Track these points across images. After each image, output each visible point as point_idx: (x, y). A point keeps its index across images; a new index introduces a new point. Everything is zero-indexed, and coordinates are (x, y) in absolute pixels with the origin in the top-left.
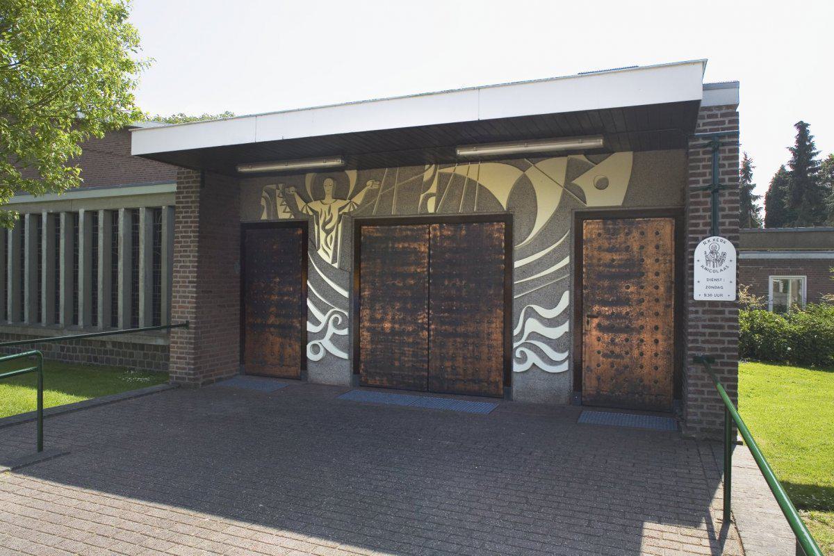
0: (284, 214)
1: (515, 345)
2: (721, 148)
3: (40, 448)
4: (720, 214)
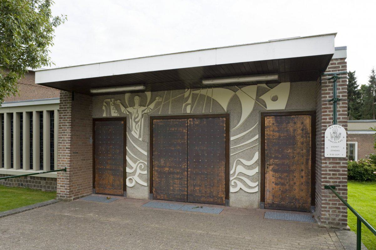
0: (114, 114)
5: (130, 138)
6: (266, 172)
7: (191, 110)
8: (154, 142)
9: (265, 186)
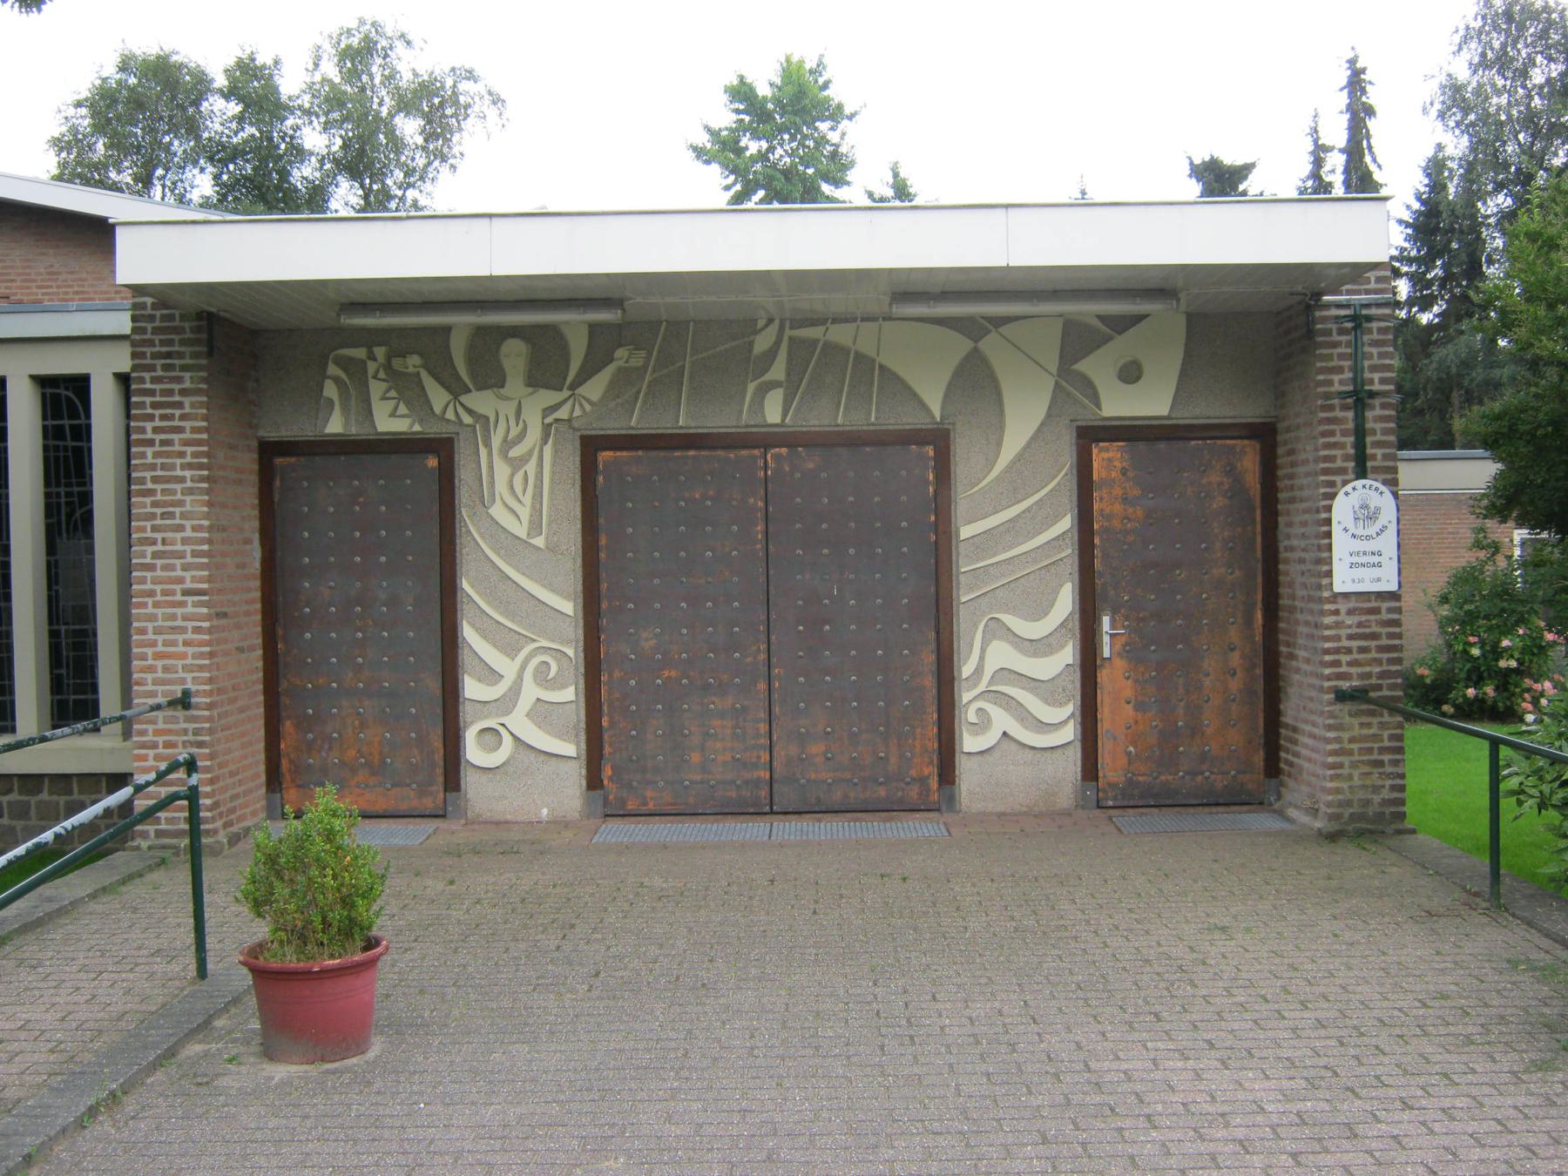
0: (390, 420)
1: (966, 697)
2: (1366, 325)
3: (202, 972)
4: (1369, 439)
6: (1098, 662)
7: (785, 413)
8: (602, 555)
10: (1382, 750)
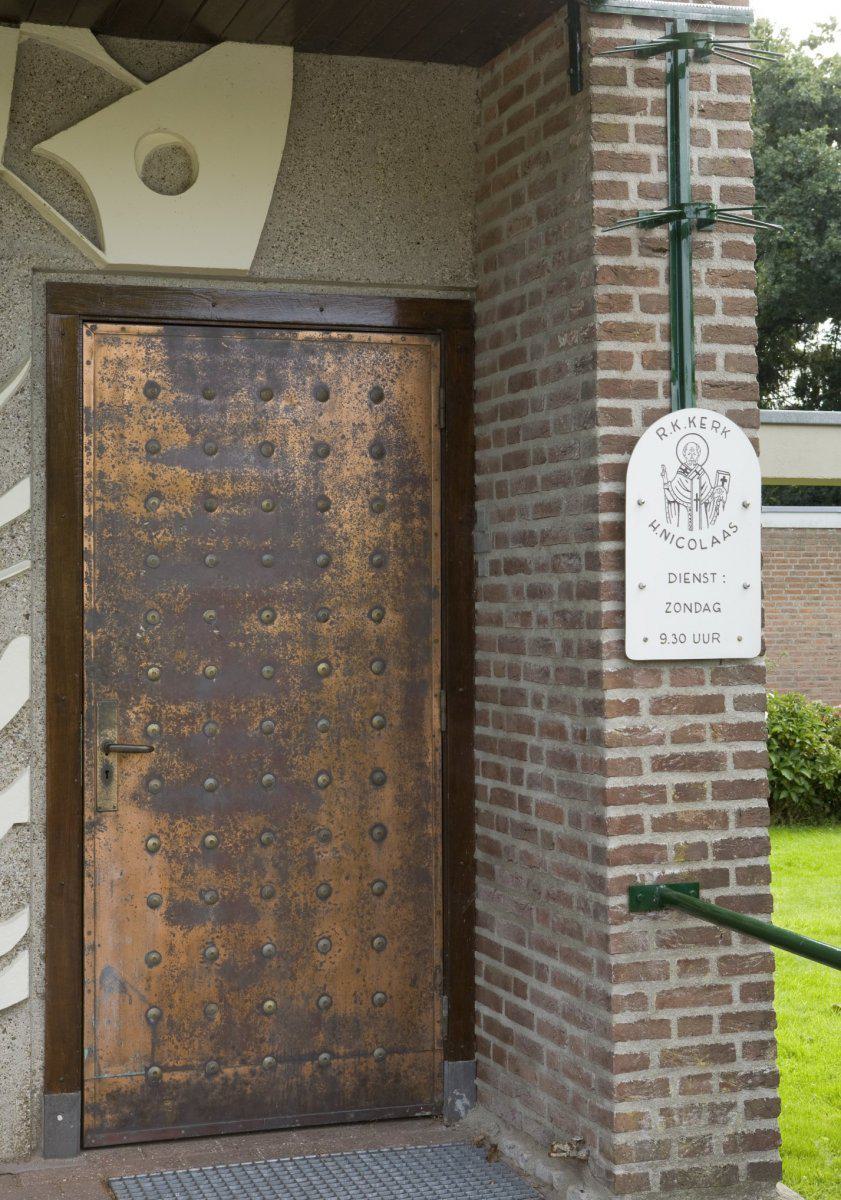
5: (672, 214)
6: (88, 814)
9: (88, 940)
10: (731, 1022)
